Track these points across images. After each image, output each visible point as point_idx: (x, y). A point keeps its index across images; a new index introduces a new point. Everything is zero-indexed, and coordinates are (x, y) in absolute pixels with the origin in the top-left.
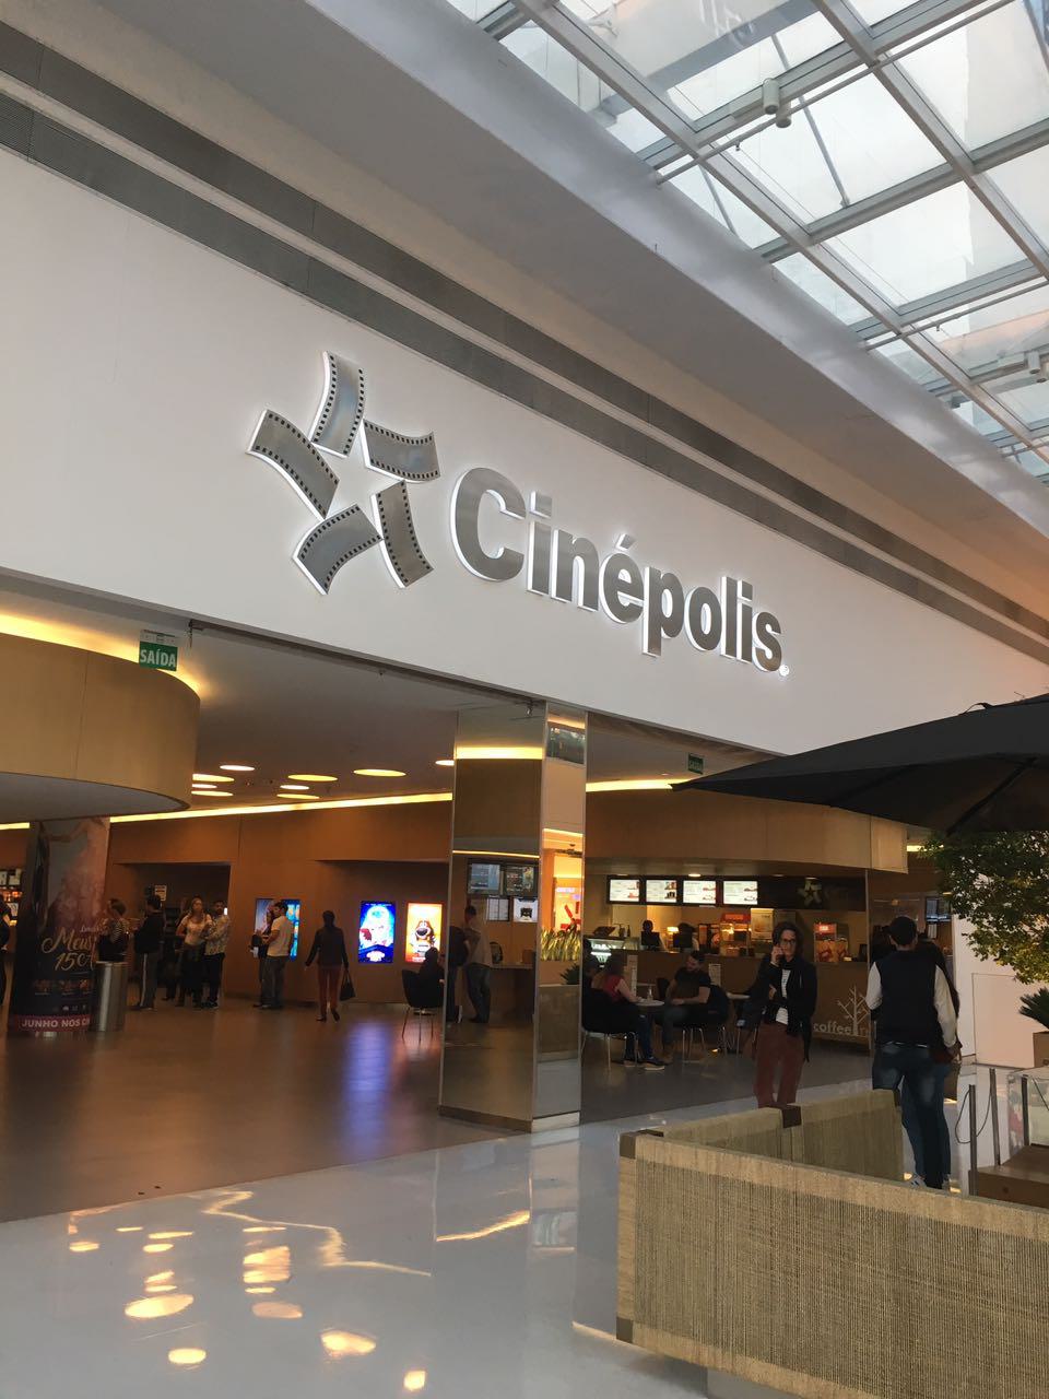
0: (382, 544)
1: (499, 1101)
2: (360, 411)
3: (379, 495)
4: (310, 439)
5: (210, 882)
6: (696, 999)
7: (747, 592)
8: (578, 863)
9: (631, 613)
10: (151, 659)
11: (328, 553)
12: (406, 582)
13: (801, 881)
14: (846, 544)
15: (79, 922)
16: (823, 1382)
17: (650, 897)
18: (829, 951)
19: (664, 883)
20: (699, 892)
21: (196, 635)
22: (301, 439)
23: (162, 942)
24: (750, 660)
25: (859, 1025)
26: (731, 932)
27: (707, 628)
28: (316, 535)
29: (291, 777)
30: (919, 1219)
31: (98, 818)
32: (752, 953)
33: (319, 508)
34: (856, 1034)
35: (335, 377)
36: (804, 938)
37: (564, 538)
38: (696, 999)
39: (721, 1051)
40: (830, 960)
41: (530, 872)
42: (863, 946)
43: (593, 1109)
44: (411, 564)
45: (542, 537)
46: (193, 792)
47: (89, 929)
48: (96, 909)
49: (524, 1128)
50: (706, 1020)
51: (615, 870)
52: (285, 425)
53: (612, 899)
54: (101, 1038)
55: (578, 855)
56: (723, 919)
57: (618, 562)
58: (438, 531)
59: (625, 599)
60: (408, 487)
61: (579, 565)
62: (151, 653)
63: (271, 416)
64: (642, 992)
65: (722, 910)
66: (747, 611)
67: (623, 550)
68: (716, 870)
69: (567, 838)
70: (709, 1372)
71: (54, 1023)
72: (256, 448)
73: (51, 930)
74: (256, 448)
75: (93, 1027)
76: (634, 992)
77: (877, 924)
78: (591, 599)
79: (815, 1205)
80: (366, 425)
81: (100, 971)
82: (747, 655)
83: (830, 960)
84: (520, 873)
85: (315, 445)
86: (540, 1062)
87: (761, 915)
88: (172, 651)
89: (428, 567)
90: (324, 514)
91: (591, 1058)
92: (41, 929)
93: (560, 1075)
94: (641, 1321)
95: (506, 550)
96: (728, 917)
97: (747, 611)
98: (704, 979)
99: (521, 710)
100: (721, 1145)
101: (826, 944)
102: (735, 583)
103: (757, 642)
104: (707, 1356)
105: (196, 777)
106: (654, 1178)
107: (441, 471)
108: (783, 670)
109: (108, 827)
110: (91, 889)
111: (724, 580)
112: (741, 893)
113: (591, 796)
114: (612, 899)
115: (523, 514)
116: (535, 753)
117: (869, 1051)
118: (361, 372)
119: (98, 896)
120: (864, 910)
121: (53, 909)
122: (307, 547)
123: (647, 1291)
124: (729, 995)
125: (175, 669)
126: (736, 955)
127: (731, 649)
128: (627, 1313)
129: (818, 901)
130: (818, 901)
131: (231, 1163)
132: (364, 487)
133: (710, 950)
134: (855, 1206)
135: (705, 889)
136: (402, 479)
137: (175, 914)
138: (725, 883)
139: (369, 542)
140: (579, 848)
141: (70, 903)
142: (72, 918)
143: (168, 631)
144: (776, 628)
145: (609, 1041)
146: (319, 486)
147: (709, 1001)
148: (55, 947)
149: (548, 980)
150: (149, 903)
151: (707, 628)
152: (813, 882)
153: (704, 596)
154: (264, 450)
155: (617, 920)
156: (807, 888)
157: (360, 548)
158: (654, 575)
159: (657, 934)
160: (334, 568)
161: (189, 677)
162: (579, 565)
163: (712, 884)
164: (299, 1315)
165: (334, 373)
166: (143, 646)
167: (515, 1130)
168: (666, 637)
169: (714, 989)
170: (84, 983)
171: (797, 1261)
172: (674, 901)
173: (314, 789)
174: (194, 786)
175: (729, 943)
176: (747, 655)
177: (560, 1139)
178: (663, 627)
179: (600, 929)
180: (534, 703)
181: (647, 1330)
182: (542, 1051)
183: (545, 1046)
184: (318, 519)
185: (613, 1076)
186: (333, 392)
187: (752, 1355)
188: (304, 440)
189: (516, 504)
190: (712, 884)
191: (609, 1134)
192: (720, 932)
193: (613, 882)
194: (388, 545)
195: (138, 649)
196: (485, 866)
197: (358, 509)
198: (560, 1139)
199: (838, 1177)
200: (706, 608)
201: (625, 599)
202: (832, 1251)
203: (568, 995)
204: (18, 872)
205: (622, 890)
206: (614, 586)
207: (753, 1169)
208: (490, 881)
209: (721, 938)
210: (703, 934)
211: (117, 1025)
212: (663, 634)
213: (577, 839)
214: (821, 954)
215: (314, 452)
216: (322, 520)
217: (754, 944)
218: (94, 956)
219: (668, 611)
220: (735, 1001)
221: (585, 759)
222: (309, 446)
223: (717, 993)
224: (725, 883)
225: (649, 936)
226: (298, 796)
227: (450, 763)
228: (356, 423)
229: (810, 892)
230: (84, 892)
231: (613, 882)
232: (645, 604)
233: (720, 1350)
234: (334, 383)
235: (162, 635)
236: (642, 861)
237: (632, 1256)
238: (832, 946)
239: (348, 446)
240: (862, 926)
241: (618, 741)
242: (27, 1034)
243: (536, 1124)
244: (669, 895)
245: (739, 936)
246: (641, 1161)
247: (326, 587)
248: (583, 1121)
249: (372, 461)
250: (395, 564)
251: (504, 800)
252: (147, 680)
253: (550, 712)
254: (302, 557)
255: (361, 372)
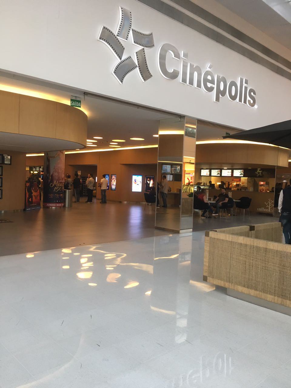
0: (138, 68)
1: (170, 225)
2: (130, 26)
3: (137, 53)
4: (116, 35)
5: (92, 170)
6: (224, 201)
7: (246, 83)
8: (193, 166)
9: (210, 90)
10: (74, 104)
11: (122, 71)
12: (145, 80)
13: (256, 170)
14: (278, 67)
15: (59, 179)
16: (258, 292)
17: (212, 174)
18: (263, 189)
19: (216, 170)
20: (226, 173)
21: (86, 97)
22: (113, 35)
23: (81, 186)
24: (246, 103)
25: (270, 209)
26: (235, 184)
27: (233, 94)
28: (119, 64)
29: (113, 140)
30: (288, 252)
31: (61, 151)
32: (241, 189)
33: (119, 57)
34: (269, 211)
35: (123, 19)
36: (256, 185)
37: (191, 66)
38: (224, 201)
39: (231, 215)
40: (263, 192)
41: (179, 167)
42: (273, 188)
43: (196, 228)
44: (146, 74)
45: (185, 67)
46: (87, 145)
47: (61, 181)
48: (63, 176)
49: (178, 232)
50: (226, 207)
51: (202, 167)
52: (107, 29)
53: (201, 175)
54: (67, 209)
55: (193, 163)
56: (233, 180)
57: (207, 73)
58: (154, 66)
59: (209, 85)
60: (145, 50)
61: (196, 74)
62: (74, 102)
63: (104, 28)
64: (210, 199)
65: (232, 178)
66: (246, 88)
67: (209, 70)
68: (232, 167)
69: (189, 159)
70: (227, 289)
71: (54, 205)
72: (100, 38)
73: (52, 181)
74: (100, 38)
75: (64, 206)
76: (207, 200)
77: (277, 182)
78: (199, 85)
79: (258, 249)
80: (132, 30)
81: (65, 192)
82: (245, 102)
83: (263, 192)
84: (176, 168)
85: (117, 37)
86: (182, 217)
87: (244, 179)
88: (79, 102)
89: (151, 75)
90: (121, 59)
91: (196, 215)
92: (49, 181)
93: (187, 220)
94: (209, 276)
95: (174, 69)
96: (234, 180)
97: (246, 88)
98: (227, 196)
99: (178, 119)
100: (233, 234)
101: (262, 187)
102: (243, 79)
103: (248, 98)
104: (227, 285)
105: (88, 141)
106: (213, 242)
107: (155, 45)
108: (256, 107)
109: (65, 155)
110: (62, 171)
111: (239, 78)
112: (237, 173)
113: (197, 145)
114: (201, 175)
115: (179, 58)
116: (182, 132)
117: (272, 215)
118: (130, 13)
119: (63, 172)
120: (275, 178)
121: (52, 176)
122: (116, 69)
123: (232, 251)
124: (234, 200)
125: (80, 107)
126: (236, 190)
127: (240, 100)
128: (206, 274)
129: (261, 175)
130: (261, 175)
131: (101, 239)
132: (132, 49)
133: (229, 189)
134: (270, 249)
135: (228, 172)
136: (143, 47)
137: (85, 178)
138: (234, 170)
139: (134, 68)
140: (193, 161)
141: (56, 174)
142: (57, 178)
143: (79, 96)
144: (255, 94)
145: (200, 212)
146: (119, 50)
147: (228, 201)
148: (53, 186)
149: (184, 196)
150: (75, 175)
151: (233, 94)
152: (260, 170)
153: (233, 84)
154: (103, 39)
155: (203, 180)
156: (258, 171)
157: (130, 70)
158: (218, 77)
159: (214, 184)
160: (126, 73)
161: (84, 109)
162: (196, 74)
163: (230, 171)
164: (120, 275)
165: (123, 15)
166: (72, 100)
167: (175, 233)
168: (221, 97)
169: (229, 198)
170: (61, 195)
171: (253, 263)
172: (219, 175)
173: (120, 144)
174: (87, 143)
175: (234, 187)
176: (245, 102)
177: (187, 236)
178: (220, 93)
179: (198, 183)
180: (181, 117)
181: (211, 279)
182: (182, 214)
183: (183, 213)
184: (118, 61)
185: (201, 220)
186: (122, 22)
187: (239, 285)
188: (114, 36)
189: (177, 55)
190: (230, 171)
191: (201, 235)
192: (232, 184)
193: (202, 170)
194: (140, 69)
195: (70, 102)
196: (166, 166)
197: (130, 57)
198: (187, 236)
199: (265, 242)
200: (233, 88)
201: (209, 85)
202: (263, 260)
203: (189, 200)
204: (42, 167)
205: (205, 172)
206: (206, 81)
207: (241, 240)
208: (168, 170)
209: (232, 185)
210: (227, 185)
211: (70, 206)
212: (220, 96)
213: (193, 159)
214: (260, 190)
215: (117, 39)
216: (120, 61)
217: (241, 187)
218: (63, 188)
219: (222, 88)
220: (236, 202)
221: (196, 137)
222: (116, 37)
223: (230, 200)
224: (234, 170)
225: (212, 186)
226: (114, 146)
227: (157, 136)
228: (130, 30)
229: (259, 173)
230: (60, 171)
231: (202, 170)
232: (215, 86)
233: (231, 284)
234: (123, 17)
235: (76, 97)
236: (210, 164)
237: (208, 261)
238: (264, 188)
239: (127, 37)
240: (273, 182)
241: (206, 127)
242: (48, 207)
243: (181, 231)
244: (218, 174)
245: (237, 185)
246: (211, 238)
247: (122, 82)
248: (193, 231)
249: (134, 42)
250: (142, 75)
251: (173, 146)
252: (71, 111)
253: (186, 123)
254: (115, 72)
255: (130, 13)
